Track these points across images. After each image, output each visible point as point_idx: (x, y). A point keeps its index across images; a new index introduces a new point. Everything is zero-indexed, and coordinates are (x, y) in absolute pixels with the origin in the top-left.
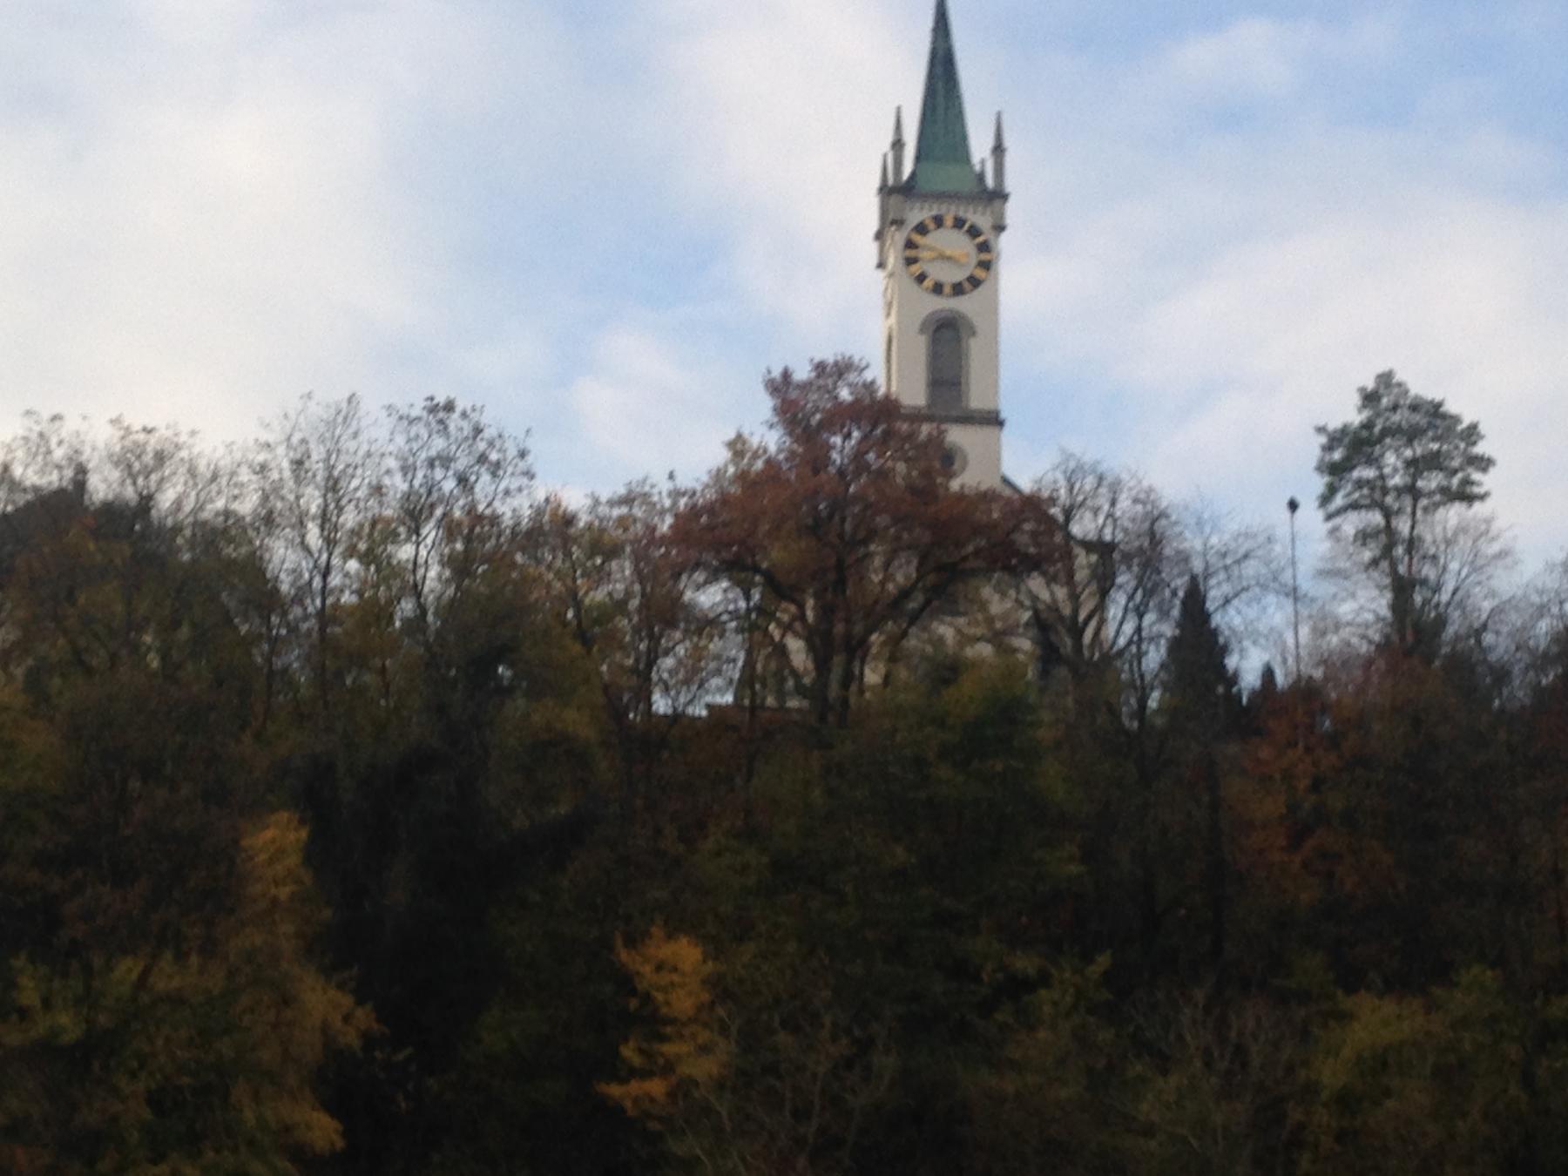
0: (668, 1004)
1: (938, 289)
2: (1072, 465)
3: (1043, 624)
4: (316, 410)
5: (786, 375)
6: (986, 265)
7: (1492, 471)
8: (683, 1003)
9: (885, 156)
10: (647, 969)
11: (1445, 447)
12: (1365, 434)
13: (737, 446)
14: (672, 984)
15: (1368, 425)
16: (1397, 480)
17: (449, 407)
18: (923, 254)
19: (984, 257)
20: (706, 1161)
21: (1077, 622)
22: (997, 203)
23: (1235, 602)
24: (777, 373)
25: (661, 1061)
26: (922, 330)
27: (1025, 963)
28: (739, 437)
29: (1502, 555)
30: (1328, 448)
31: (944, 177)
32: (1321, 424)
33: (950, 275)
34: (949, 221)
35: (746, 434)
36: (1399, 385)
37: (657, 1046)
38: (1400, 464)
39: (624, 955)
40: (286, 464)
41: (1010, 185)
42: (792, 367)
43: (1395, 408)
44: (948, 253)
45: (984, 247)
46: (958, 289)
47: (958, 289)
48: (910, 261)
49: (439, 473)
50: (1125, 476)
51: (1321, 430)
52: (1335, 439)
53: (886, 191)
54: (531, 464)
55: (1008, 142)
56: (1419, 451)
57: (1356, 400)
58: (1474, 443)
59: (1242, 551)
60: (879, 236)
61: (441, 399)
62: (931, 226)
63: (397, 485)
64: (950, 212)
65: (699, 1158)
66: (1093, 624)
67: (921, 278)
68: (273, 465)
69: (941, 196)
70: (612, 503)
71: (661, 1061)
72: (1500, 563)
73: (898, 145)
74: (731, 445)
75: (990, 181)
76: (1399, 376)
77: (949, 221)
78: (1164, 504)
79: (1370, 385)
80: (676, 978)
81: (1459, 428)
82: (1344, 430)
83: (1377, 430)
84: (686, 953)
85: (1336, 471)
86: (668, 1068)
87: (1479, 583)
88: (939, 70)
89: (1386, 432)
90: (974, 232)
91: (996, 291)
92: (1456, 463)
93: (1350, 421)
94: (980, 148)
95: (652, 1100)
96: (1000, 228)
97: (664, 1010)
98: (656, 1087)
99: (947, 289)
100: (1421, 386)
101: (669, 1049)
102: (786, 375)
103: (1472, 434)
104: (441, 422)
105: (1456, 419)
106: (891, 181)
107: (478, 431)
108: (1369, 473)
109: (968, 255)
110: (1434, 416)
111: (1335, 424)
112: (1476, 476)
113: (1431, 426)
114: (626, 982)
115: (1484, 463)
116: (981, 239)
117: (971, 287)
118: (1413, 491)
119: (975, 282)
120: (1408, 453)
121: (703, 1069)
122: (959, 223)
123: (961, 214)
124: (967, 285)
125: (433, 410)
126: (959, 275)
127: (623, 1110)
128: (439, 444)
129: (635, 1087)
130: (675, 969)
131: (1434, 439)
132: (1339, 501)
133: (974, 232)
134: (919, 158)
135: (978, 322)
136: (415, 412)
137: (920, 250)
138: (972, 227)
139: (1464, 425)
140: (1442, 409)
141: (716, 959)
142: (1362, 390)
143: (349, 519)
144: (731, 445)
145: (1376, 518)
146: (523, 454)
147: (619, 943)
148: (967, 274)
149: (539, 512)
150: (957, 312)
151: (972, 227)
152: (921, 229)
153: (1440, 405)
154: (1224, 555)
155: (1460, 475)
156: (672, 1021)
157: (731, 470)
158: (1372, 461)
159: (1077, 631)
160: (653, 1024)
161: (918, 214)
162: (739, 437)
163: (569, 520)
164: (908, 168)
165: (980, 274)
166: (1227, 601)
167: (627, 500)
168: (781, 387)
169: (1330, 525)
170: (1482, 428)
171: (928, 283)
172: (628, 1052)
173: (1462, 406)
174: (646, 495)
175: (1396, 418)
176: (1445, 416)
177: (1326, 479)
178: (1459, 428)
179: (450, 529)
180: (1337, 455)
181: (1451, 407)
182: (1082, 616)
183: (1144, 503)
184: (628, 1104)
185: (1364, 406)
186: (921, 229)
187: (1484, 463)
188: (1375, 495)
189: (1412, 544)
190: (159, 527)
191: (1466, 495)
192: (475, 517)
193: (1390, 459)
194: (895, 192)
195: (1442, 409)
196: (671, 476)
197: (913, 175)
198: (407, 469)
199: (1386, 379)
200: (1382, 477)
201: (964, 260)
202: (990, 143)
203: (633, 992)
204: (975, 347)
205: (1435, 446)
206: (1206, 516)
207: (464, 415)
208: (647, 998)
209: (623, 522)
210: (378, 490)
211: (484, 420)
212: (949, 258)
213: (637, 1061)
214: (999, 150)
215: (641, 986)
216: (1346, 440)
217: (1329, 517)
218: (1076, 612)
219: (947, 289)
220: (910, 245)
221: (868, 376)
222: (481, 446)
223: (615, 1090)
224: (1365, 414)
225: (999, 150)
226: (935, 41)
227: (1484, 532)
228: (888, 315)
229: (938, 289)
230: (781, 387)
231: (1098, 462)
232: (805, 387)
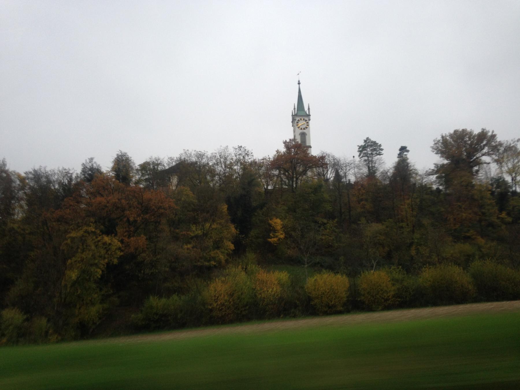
0: (276, 228)
2: (323, 152)
3: (319, 174)
4: (222, 148)
5: (286, 141)
6: (308, 125)
7: (383, 151)
8: (279, 227)
9: (292, 110)
10: (273, 223)
11: (376, 148)
12: (364, 146)
13: (278, 151)
14: (277, 225)
15: (365, 145)
16: (370, 153)
17: (241, 147)
19: (308, 124)
20: (374, 268)
22: (309, 116)
23: (351, 170)
24: (285, 141)
25: (276, 236)
26: (300, 135)
27: (325, 221)
28: (278, 150)
29: (383, 163)
30: (359, 148)
31: (301, 113)
32: (358, 145)
34: (302, 119)
35: (279, 150)
36: (370, 139)
37: (275, 234)
38: (370, 150)
39: (270, 221)
40: (218, 155)
41: (311, 114)
42: (287, 140)
45: (307, 123)
46: (304, 129)
49: (240, 156)
50: (330, 154)
51: (358, 146)
52: (360, 147)
53: (292, 115)
55: (310, 108)
56: (373, 148)
57: (363, 141)
58: (380, 147)
59: (351, 163)
61: (240, 146)
62: (300, 120)
63: (235, 158)
65: (373, 267)
66: (326, 174)
68: (216, 156)
70: (261, 160)
71: (276, 236)
72: (383, 164)
73: (295, 109)
74: (276, 151)
75: (307, 113)
76: (369, 138)
77: (302, 119)
78: (336, 158)
79: (365, 139)
80: (277, 224)
81: (378, 145)
82: (362, 146)
83: (366, 146)
84: (278, 221)
85: (361, 152)
86: (277, 237)
87: (380, 167)
89: (368, 146)
90: (306, 121)
92: (378, 150)
94: (306, 109)
95: (275, 241)
96: (309, 120)
97: (276, 229)
98: (275, 239)
99: (303, 129)
100: (373, 139)
101: (277, 234)
102: (286, 141)
103: (380, 145)
104: (240, 149)
105: (378, 144)
106: (294, 114)
107: (245, 150)
108: (366, 152)
110: (375, 143)
111: (360, 145)
112: (381, 151)
113: (374, 145)
114: (270, 225)
115: (382, 150)
116: (307, 122)
118: (372, 154)
119: (306, 128)
120: (371, 149)
121: (282, 236)
122: (304, 119)
124: (305, 128)
125: (239, 147)
127: (271, 243)
128: (240, 152)
129: (273, 239)
130: (277, 223)
131: (375, 147)
132: (361, 155)
133: (306, 121)
134: (297, 111)
135: (308, 134)
136: (236, 148)
138: (306, 120)
139: (379, 144)
140: (376, 142)
141: (282, 221)
142: (364, 140)
143: (228, 162)
144: (276, 151)
145: (366, 158)
146: (252, 153)
148: (305, 127)
151: (306, 120)
153: (375, 142)
154: (349, 163)
155: (379, 151)
156: (277, 230)
157: (277, 155)
158: (365, 150)
159: (324, 176)
160: (275, 231)
161: (297, 119)
162: (278, 150)
163: (256, 163)
164: (296, 113)
165: (307, 126)
166: (349, 170)
167: (263, 159)
168: (285, 143)
169: (360, 159)
170: (382, 145)
172: (271, 235)
173: (379, 142)
174: (266, 159)
175: (369, 144)
176: (376, 143)
177: (359, 153)
178: (378, 145)
179: (241, 164)
180: (361, 149)
181: (377, 142)
182: (325, 173)
183: (333, 157)
184: (272, 242)
185: (365, 142)
186: (299, 120)
187: (382, 150)
188: (366, 155)
189: (372, 161)
190: (64, 189)
191: (380, 154)
192: (244, 161)
193: (368, 149)
194: (294, 116)
195: (376, 142)
196: (269, 156)
197: (297, 113)
198: (236, 156)
199: (368, 138)
200: (367, 152)
202: (308, 108)
203: (271, 226)
204: (307, 137)
205: (375, 147)
206: (346, 158)
207: (243, 148)
208: (273, 227)
209: (263, 162)
210: (232, 159)
211: (246, 149)
213: (272, 236)
214: (309, 109)
215: (272, 226)
216: (362, 147)
217: (360, 158)
218: (324, 172)
219: (303, 129)
221: (297, 141)
222: (246, 152)
223: (270, 240)
224: (365, 143)
225: (309, 109)
226: (299, 92)
227: (380, 160)
229: (301, 129)
230: (285, 143)
231: (326, 152)
232: (288, 142)
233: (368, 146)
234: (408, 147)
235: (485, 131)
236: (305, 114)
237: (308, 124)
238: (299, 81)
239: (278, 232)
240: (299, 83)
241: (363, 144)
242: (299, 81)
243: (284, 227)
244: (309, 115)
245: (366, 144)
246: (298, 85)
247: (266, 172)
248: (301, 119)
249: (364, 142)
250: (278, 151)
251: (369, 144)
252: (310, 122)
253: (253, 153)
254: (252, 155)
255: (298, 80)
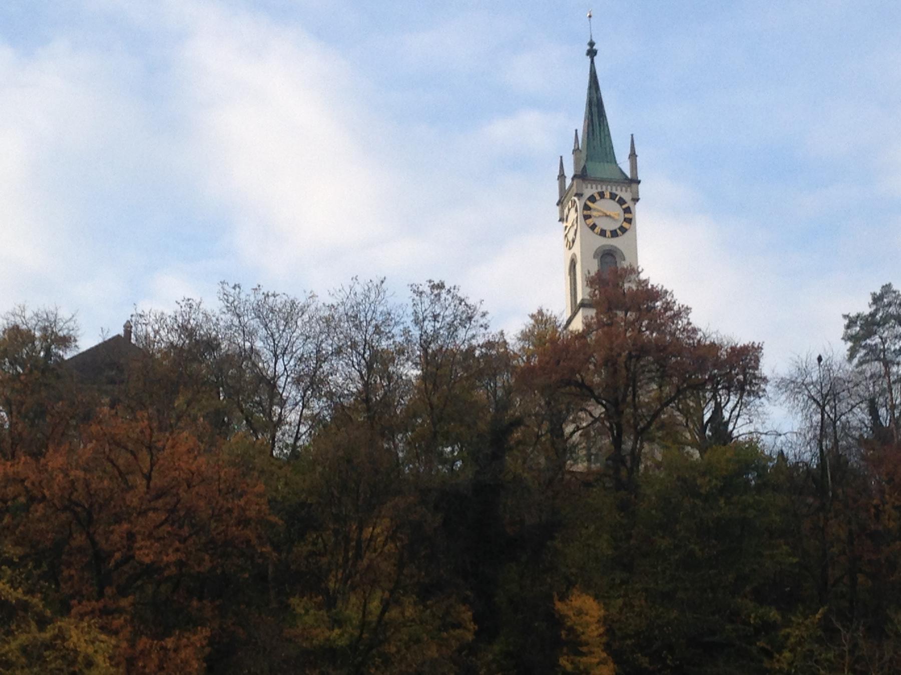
1: (603, 233)
6: (629, 221)
8: (593, 632)
10: (571, 613)
15: (873, 315)
17: (441, 286)
18: (594, 213)
19: (627, 216)
21: (703, 422)
22: (634, 185)
30: (848, 327)
31: (598, 170)
32: (846, 313)
33: (610, 226)
34: (607, 195)
35: (544, 311)
39: (559, 606)
43: (890, 304)
44: (608, 214)
45: (628, 210)
46: (614, 234)
47: (614, 234)
48: (586, 217)
51: (846, 316)
52: (852, 322)
54: (489, 321)
55: (638, 151)
60: (560, 203)
62: (598, 198)
64: (607, 190)
67: (593, 227)
69: (602, 181)
76: (894, 288)
77: (607, 195)
79: (689, 307)
85: (856, 340)
88: (595, 109)
90: (621, 202)
91: (636, 235)
93: (862, 312)
96: (636, 200)
99: (608, 234)
109: (619, 215)
111: (853, 314)
116: (624, 206)
117: (610, 236)
119: (623, 230)
122: (613, 196)
123: (614, 191)
126: (615, 226)
130: (587, 614)
133: (621, 202)
137: (592, 210)
146: (484, 315)
147: (556, 598)
148: (618, 225)
149: (489, 345)
150: (616, 247)
151: (620, 198)
152: (592, 199)
165: (626, 225)
171: (597, 230)
177: (850, 344)
186: (592, 199)
201: (617, 217)
202: (628, 151)
208: (571, 630)
212: (607, 216)
214: (633, 156)
219: (608, 234)
220: (586, 207)
224: (874, 307)
225: (633, 156)
226: (590, 88)
228: (567, 246)
229: (603, 233)
233: (885, 320)
234: (840, 339)
235: (520, 336)
236: (618, 176)
237: (627, 216)
238: (592, 44)
239: (591, 653)
240: (592, 53)
241: (867, 310)
242: (592, 44)
243: (610, 627)
244: (635, 181)
245: (877, 310)
246: (588, 59)
247: (99, 417)
248: (602, 195)
249: (871, 301)
250: (540, 319)
251: (892, 310)
252: (639, 211)
253: (488, 317)
254: (482, 321)
255: (589, 40)
